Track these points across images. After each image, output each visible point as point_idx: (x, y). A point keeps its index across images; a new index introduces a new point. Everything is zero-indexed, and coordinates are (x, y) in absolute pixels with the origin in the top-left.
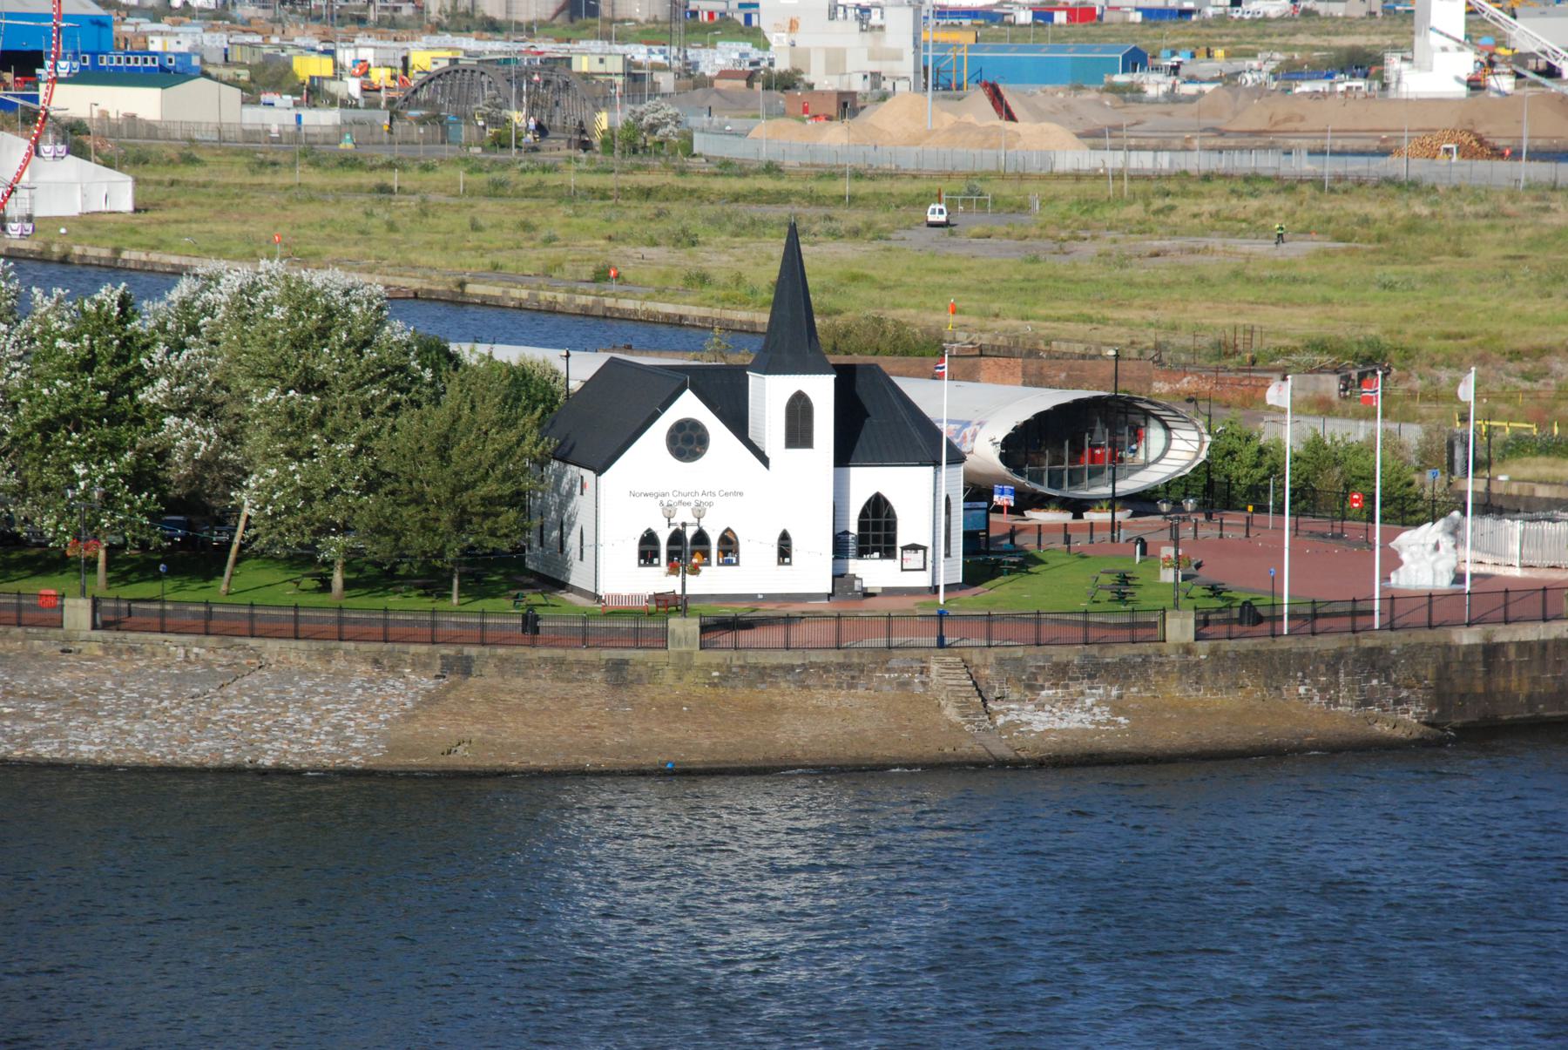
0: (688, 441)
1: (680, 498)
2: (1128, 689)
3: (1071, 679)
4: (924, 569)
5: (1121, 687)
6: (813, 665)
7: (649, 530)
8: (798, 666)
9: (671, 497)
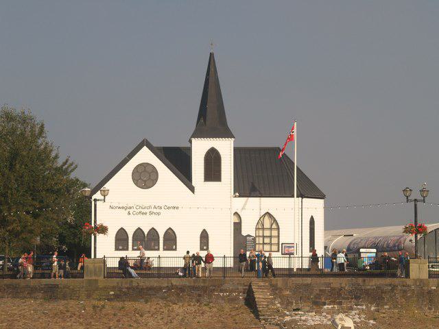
0: (145, 177)
1: (140, 210)
2: (383, 306)
3: (344, 298)
4: (278, 251)
5: (378, 305)
6: (173, 287)
7: (139, 229)
8: (164, 288)
9: (135, 209)
